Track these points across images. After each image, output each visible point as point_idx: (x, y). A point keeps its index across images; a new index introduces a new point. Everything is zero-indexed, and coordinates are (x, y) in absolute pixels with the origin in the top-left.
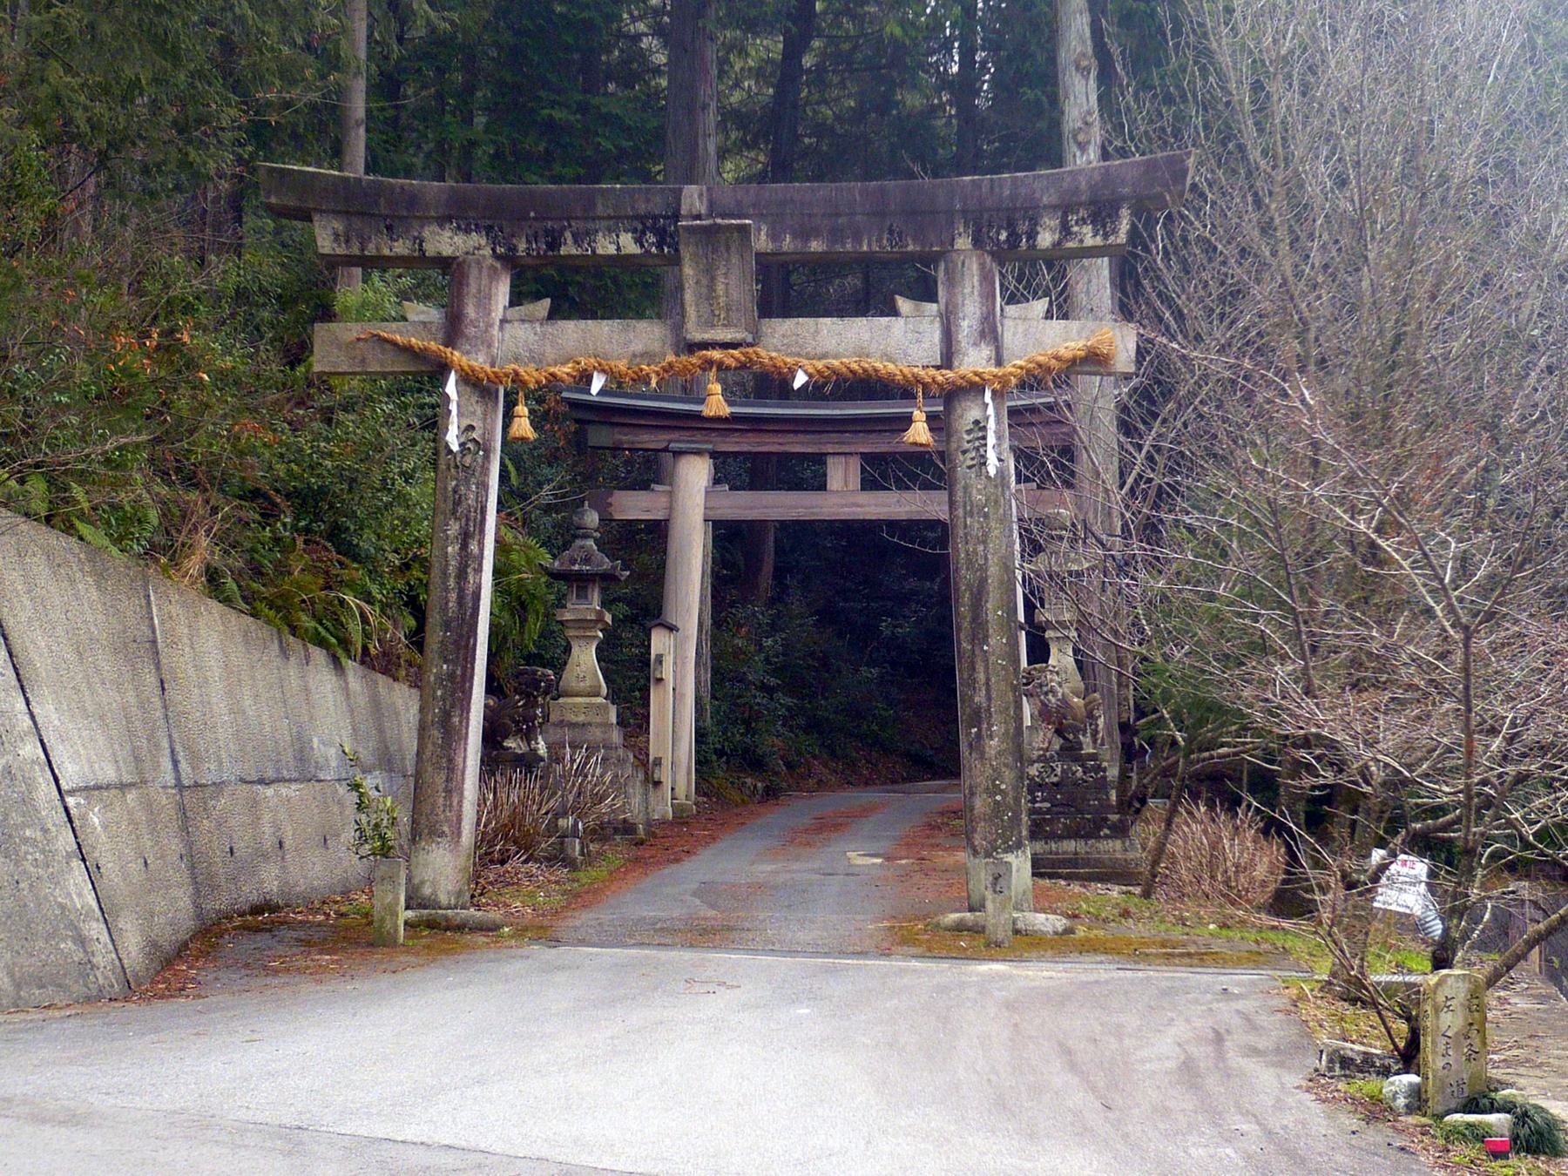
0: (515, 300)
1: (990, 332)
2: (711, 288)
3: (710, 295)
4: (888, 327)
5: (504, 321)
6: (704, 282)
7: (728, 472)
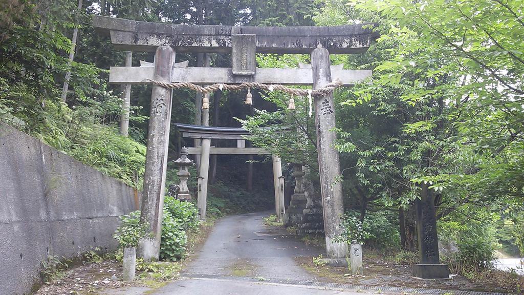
0: (177, 61)
1: (328, 76)
2: (242, 57)
3: (240, 60)
4: (296, 71)
5: (173, 67)
6: (240, 55)
7: (214, 143)
